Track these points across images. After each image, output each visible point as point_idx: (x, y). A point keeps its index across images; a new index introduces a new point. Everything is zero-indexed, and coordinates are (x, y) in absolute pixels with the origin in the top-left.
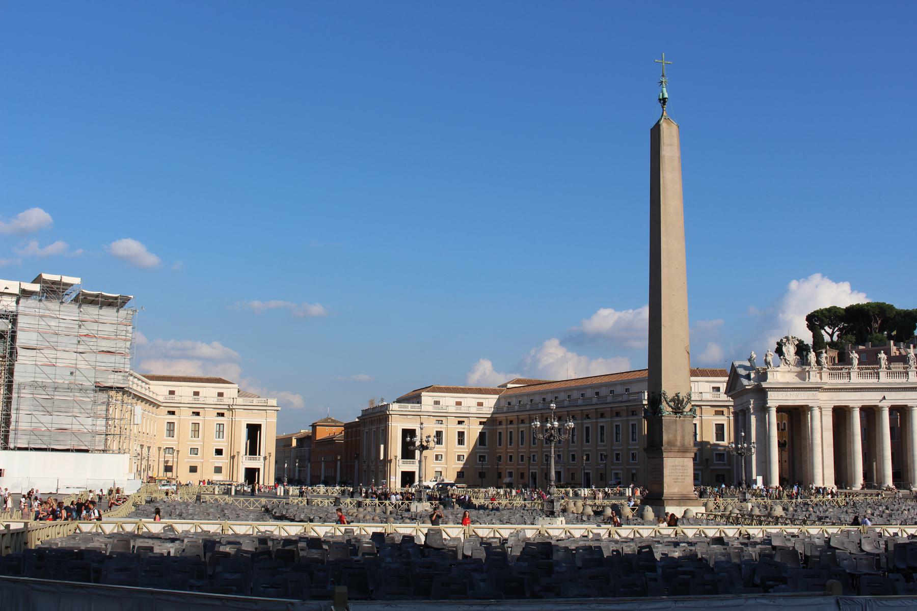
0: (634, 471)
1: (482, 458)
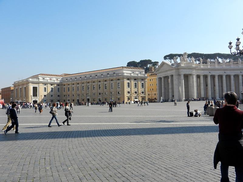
1: (52, 96)
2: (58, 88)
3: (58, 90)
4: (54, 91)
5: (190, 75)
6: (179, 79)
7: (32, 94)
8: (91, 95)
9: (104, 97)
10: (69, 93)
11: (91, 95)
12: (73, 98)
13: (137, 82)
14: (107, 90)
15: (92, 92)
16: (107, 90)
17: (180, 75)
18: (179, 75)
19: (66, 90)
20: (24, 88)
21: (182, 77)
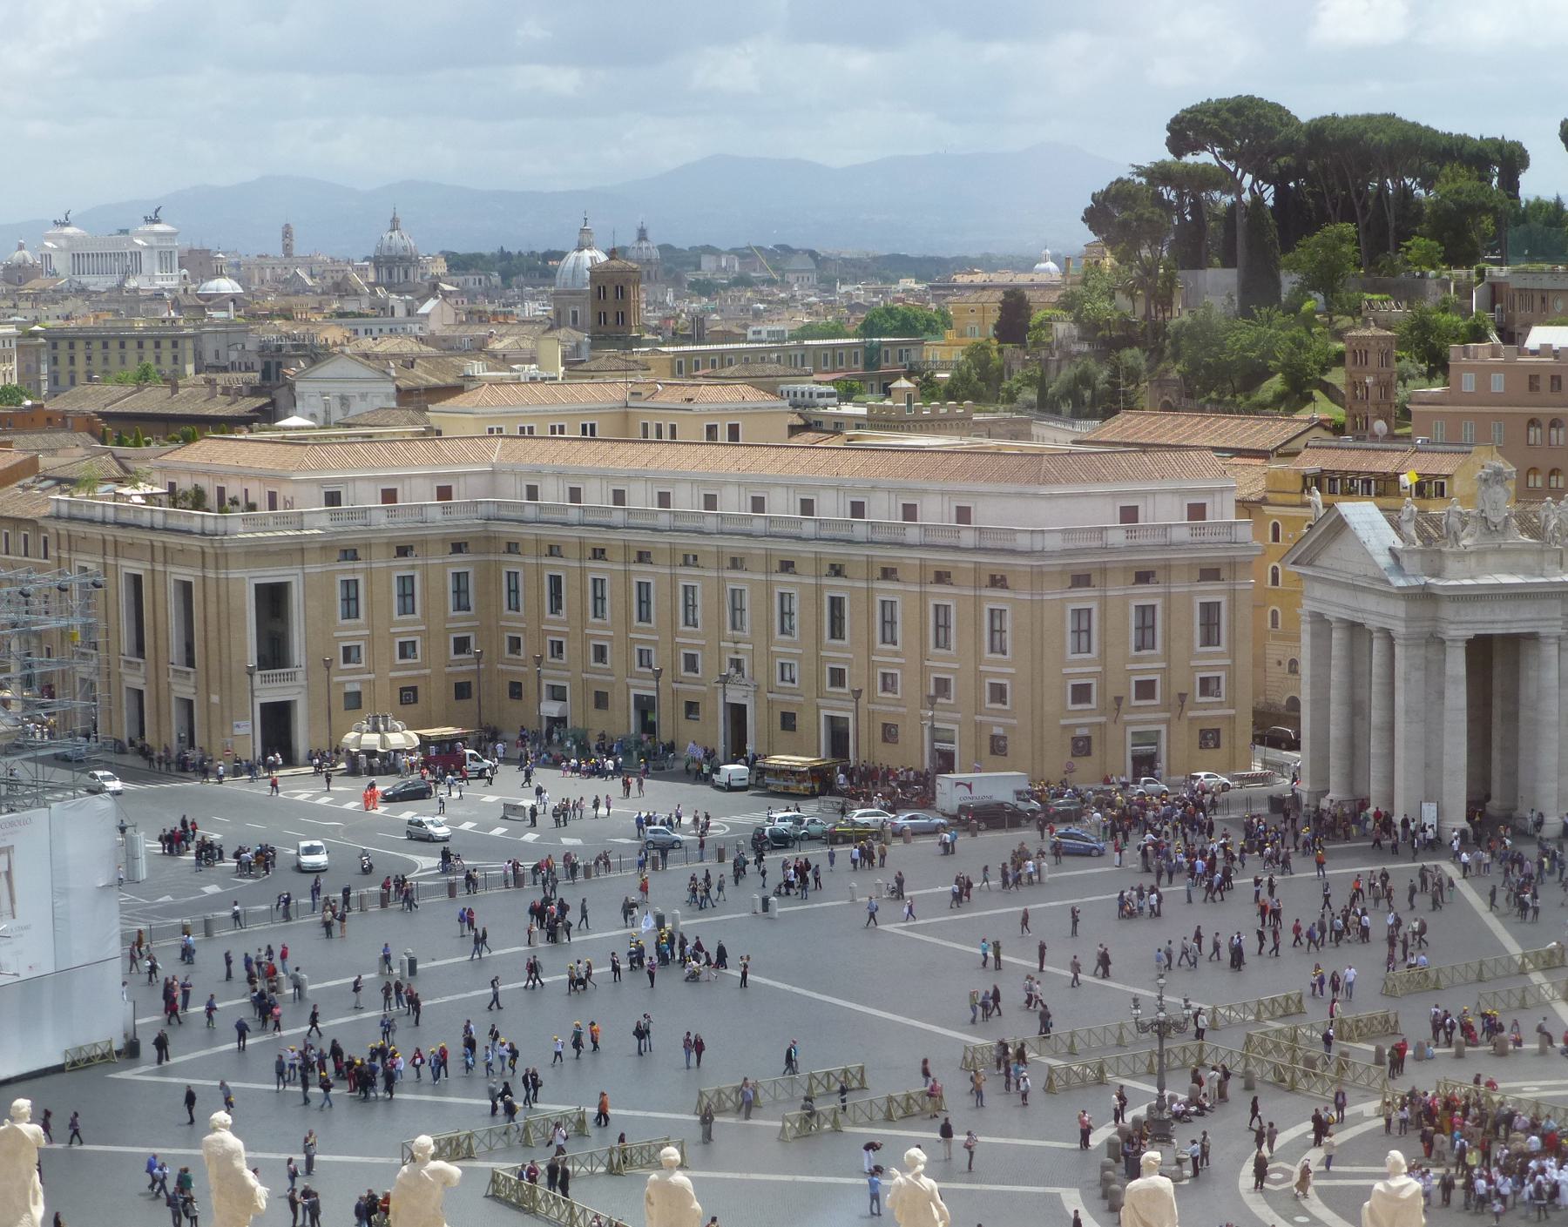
0: (998, 731)
1: (406, 650)
2: (457, 576)
3: (457, 592)
4: (426, 607)
5: (1533, 637)
6: (1434, 673)
7: (252, 661)
8: (761, 678)
9: (871, 713)
10: (556, 625)
11: (761, 678)
12: (598, 677)
13: (1156, 595)
14: (896, 654)
15: (771, 655)
16: (896, 654)
17: (1443, 642)
18: (1436, 641)
19: (534, 594)
20: (171, 586)
21: (1457, 664)
